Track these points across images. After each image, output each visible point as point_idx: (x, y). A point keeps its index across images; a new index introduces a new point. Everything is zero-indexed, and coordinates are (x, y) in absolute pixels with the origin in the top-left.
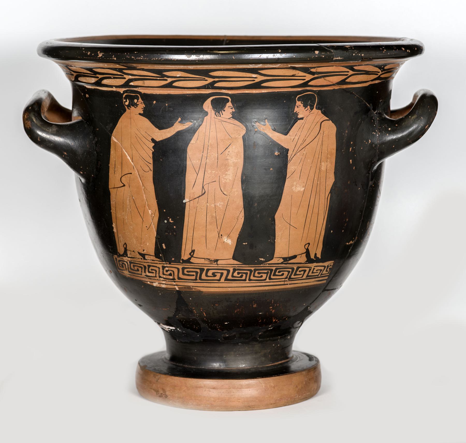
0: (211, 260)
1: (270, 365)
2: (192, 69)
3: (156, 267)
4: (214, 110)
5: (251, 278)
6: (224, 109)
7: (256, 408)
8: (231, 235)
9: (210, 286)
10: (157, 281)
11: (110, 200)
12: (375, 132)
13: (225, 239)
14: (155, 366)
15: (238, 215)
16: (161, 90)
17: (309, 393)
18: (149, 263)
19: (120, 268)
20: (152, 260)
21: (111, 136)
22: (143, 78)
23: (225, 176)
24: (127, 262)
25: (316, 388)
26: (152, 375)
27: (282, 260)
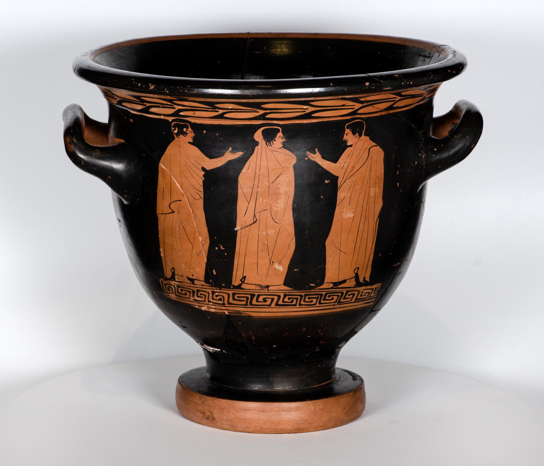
0: (262, 286)
1: (316, 386)
2: (245, 101)
3: (206, 292)
4: (265, 140)
5: (301, 303)
6: (275, 139)
7: (305, 431)
8: (282, 261)
9: (260, 311)
10: (206, 305)
11: (158, 225)
12: (421, 153)
13: (276, 266)
14: (199, 387)
15: (289, 243)
16: (211, 120)
17: (356, 414)
18: (198, 288)
19: (167, 291)
20: (202, 285)
21: (159, 163)
22: (194, 109)
23: (277, 205)
24: (174, 286)
25: (362, 408)
26: (197, 397)
27: (332, 285)
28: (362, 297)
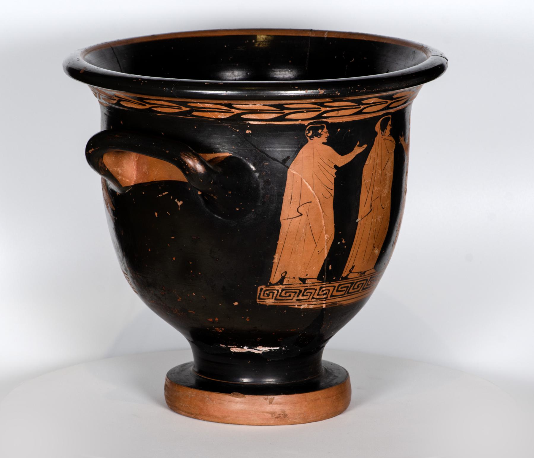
5: (314, 297)
20: (312, 283)
22: (213, 111)
28: (362, 282)
